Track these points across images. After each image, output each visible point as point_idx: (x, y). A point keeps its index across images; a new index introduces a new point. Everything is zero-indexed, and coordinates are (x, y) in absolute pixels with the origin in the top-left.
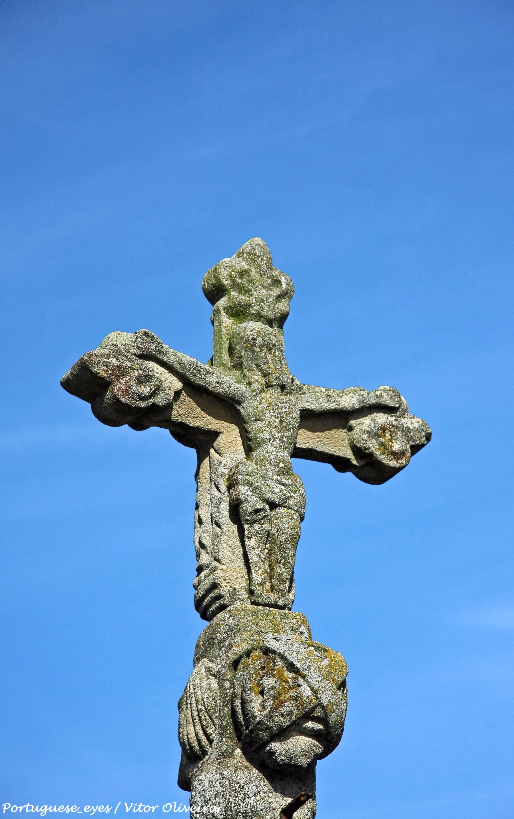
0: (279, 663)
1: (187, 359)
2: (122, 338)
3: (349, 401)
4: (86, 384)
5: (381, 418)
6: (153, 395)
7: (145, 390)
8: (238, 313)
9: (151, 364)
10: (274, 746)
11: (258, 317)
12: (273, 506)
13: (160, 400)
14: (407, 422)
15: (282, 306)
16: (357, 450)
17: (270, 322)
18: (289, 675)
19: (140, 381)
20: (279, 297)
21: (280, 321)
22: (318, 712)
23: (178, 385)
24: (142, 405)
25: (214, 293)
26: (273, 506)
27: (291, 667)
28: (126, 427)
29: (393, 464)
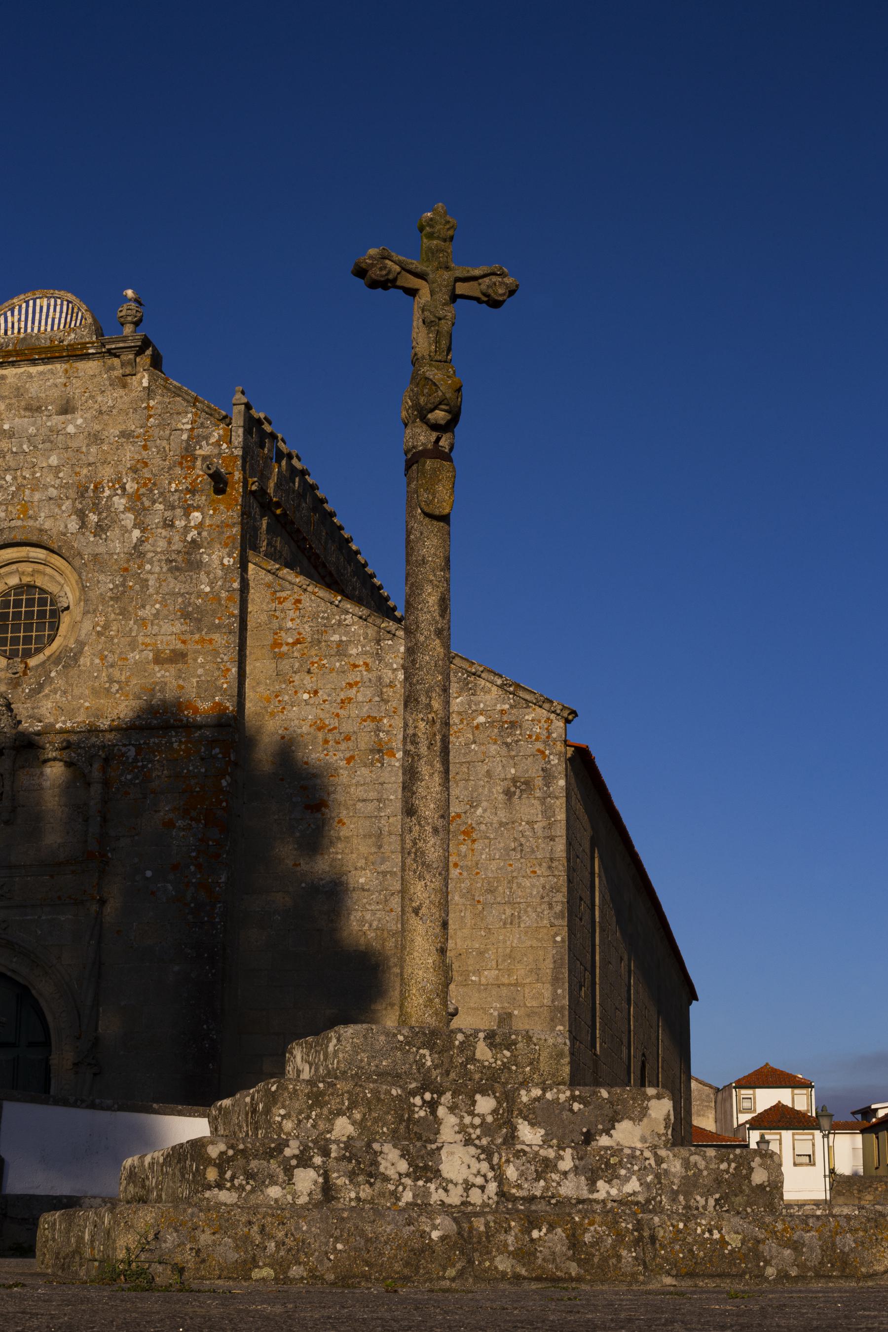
0: (430, 383)
1: (401, 258)
2: (372, 251)
3: (477, 272)
4: (360, 272)
5: (494, 279)
6: (387, 274)
7: (384, 272)
8: (431, 236)
9: (387, 261)
10: (429, 416)
11: (438, 238)
12: (440, 319)
13: (391, 277)
14: (506, 280)
15: (451, 233)
16: (484, 294)
17: (445, 240)
18: (434, 388)
19: (381, 269)
20: (448, 229)
21: (451, 238)
22: (446, 402)
23: (398, 269)
24: (382, 279)
25: (421, 229)
26: (440, 319)
27: (435, 384)
28: (380, 289)
29: (501, 299)
